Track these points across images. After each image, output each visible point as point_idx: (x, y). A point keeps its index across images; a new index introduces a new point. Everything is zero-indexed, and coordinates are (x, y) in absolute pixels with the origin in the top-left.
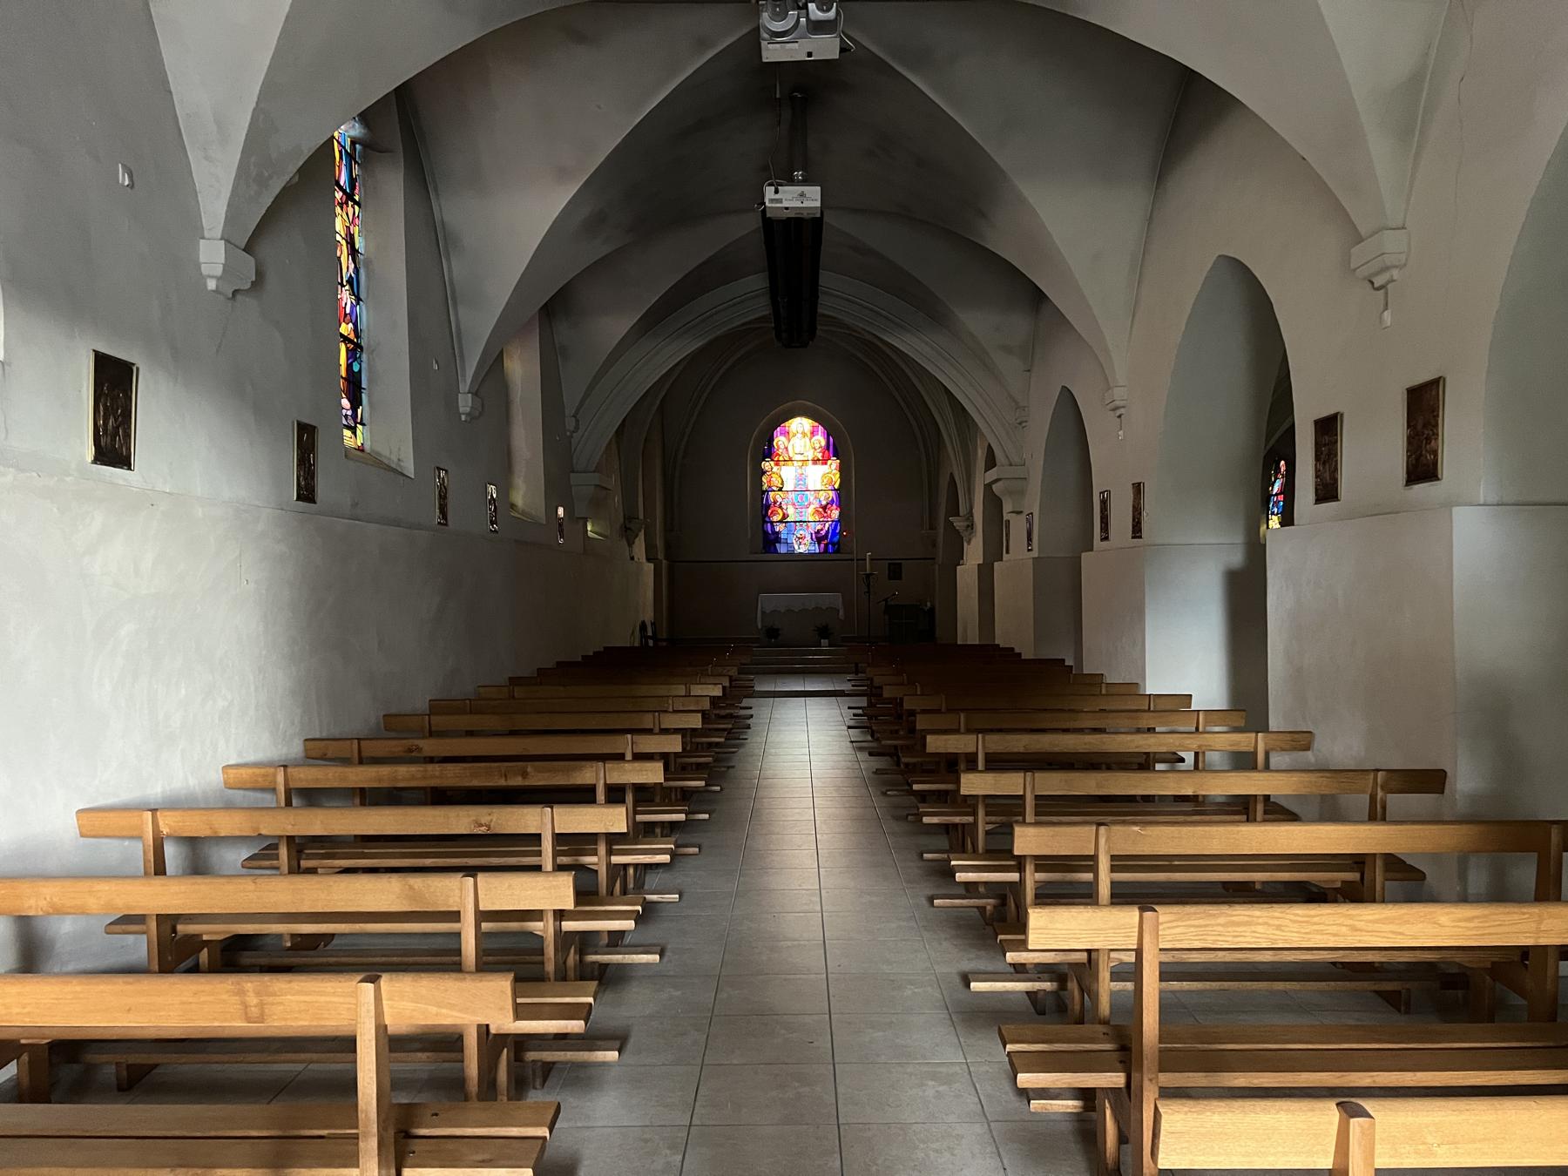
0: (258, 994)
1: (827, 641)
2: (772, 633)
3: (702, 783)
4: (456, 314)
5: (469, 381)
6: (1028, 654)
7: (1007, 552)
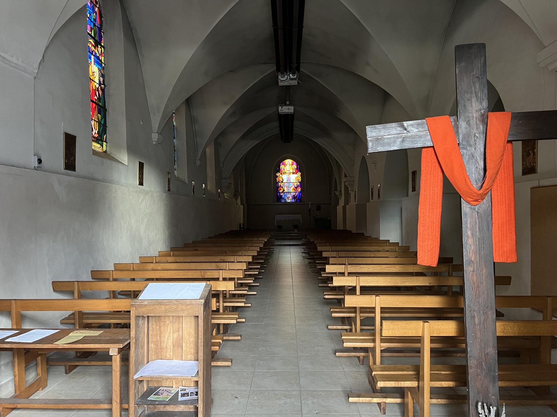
0: (204, 273)
1: (297, 230)
2: (280, 227)
3: (263, 261)
4: (196, 139)
5: (199, 157)
6: (354, 231)
7: (350, 202)
